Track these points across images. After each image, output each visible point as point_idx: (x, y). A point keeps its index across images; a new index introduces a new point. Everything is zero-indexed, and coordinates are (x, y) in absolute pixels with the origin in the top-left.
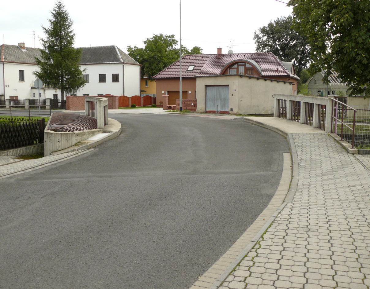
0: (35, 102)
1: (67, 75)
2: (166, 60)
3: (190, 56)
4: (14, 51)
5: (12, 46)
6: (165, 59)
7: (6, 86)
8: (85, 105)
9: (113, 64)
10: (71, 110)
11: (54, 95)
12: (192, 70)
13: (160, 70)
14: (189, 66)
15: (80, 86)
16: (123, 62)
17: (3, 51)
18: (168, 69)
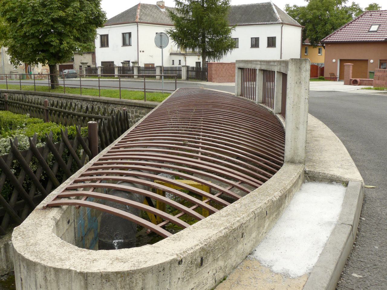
0: (169, 70)
1: (211, 34)
2: (334, 21)
3: (372, 13)
4: (151, 11)
5: (150, 5)
6: (333, 19)
7: (140, 51)
8: (236, 75)
9: (268, 24)
10: (214, 82)
11: (196, 62)
12: (377, 31)
13: (327, 34)
14: (372, 25)
15: (228, 50)
16: (281, 22)
17: (139, 11)
18: (342, 30)
